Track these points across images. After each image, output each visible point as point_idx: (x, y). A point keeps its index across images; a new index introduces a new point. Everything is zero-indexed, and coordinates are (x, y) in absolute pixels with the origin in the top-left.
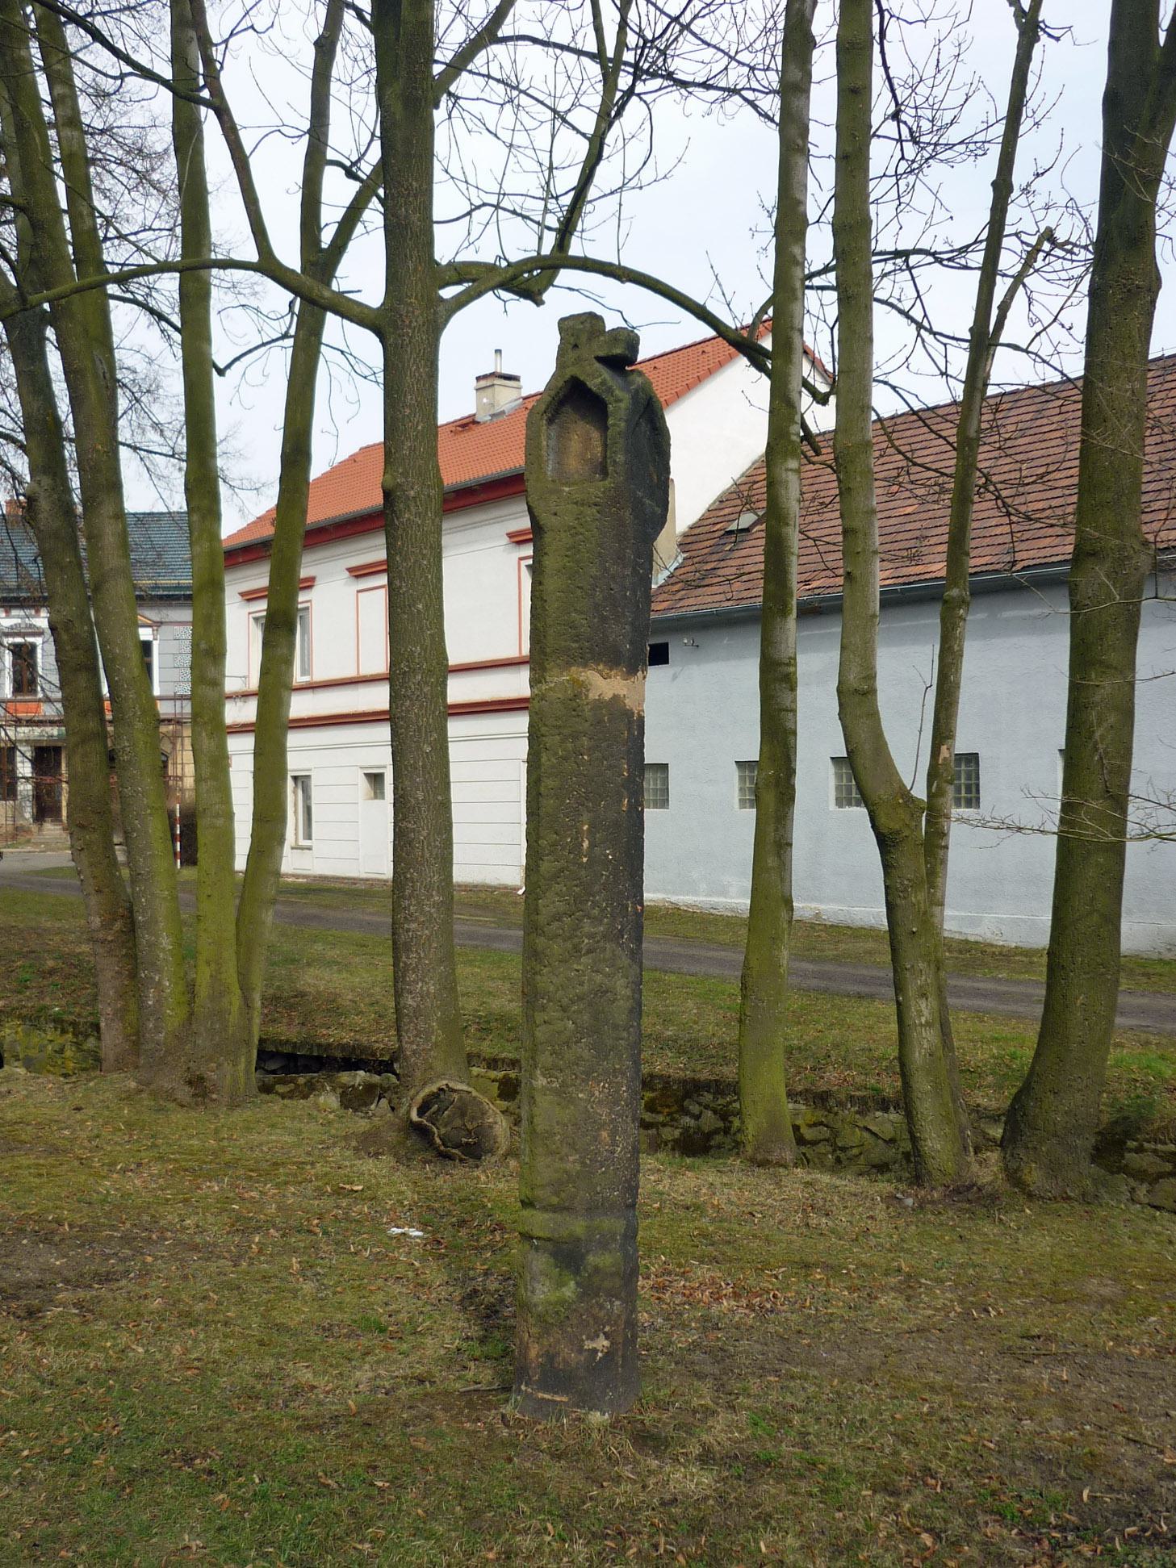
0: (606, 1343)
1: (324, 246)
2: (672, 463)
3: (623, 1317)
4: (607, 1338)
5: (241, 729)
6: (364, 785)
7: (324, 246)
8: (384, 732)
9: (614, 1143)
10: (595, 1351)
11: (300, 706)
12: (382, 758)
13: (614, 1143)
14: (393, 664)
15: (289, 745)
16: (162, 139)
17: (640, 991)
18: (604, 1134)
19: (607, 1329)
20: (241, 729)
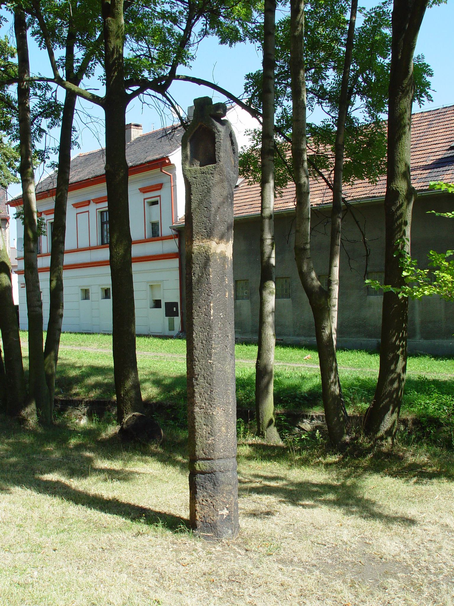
0: (227, 512)
1: (274, 264)
2: (197, 78)
3: (233, 502)
4: (227, 510)
5: (44, 270)
6: (80, 295)
7: (274, 264)
8: (107, 270)
9: (227, 432)
10: (223, 515)
11: (68, 259)
12: (107, 282)
13: (227, 432)
14: (130, 247)
15: (63, 276)
16: (13, 44)
17: (235, 370)
18: (223, 428)
19: (227, 506)
20: (44, 270)
